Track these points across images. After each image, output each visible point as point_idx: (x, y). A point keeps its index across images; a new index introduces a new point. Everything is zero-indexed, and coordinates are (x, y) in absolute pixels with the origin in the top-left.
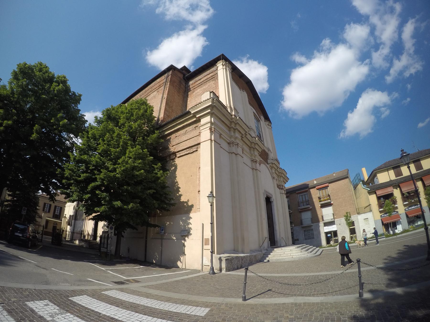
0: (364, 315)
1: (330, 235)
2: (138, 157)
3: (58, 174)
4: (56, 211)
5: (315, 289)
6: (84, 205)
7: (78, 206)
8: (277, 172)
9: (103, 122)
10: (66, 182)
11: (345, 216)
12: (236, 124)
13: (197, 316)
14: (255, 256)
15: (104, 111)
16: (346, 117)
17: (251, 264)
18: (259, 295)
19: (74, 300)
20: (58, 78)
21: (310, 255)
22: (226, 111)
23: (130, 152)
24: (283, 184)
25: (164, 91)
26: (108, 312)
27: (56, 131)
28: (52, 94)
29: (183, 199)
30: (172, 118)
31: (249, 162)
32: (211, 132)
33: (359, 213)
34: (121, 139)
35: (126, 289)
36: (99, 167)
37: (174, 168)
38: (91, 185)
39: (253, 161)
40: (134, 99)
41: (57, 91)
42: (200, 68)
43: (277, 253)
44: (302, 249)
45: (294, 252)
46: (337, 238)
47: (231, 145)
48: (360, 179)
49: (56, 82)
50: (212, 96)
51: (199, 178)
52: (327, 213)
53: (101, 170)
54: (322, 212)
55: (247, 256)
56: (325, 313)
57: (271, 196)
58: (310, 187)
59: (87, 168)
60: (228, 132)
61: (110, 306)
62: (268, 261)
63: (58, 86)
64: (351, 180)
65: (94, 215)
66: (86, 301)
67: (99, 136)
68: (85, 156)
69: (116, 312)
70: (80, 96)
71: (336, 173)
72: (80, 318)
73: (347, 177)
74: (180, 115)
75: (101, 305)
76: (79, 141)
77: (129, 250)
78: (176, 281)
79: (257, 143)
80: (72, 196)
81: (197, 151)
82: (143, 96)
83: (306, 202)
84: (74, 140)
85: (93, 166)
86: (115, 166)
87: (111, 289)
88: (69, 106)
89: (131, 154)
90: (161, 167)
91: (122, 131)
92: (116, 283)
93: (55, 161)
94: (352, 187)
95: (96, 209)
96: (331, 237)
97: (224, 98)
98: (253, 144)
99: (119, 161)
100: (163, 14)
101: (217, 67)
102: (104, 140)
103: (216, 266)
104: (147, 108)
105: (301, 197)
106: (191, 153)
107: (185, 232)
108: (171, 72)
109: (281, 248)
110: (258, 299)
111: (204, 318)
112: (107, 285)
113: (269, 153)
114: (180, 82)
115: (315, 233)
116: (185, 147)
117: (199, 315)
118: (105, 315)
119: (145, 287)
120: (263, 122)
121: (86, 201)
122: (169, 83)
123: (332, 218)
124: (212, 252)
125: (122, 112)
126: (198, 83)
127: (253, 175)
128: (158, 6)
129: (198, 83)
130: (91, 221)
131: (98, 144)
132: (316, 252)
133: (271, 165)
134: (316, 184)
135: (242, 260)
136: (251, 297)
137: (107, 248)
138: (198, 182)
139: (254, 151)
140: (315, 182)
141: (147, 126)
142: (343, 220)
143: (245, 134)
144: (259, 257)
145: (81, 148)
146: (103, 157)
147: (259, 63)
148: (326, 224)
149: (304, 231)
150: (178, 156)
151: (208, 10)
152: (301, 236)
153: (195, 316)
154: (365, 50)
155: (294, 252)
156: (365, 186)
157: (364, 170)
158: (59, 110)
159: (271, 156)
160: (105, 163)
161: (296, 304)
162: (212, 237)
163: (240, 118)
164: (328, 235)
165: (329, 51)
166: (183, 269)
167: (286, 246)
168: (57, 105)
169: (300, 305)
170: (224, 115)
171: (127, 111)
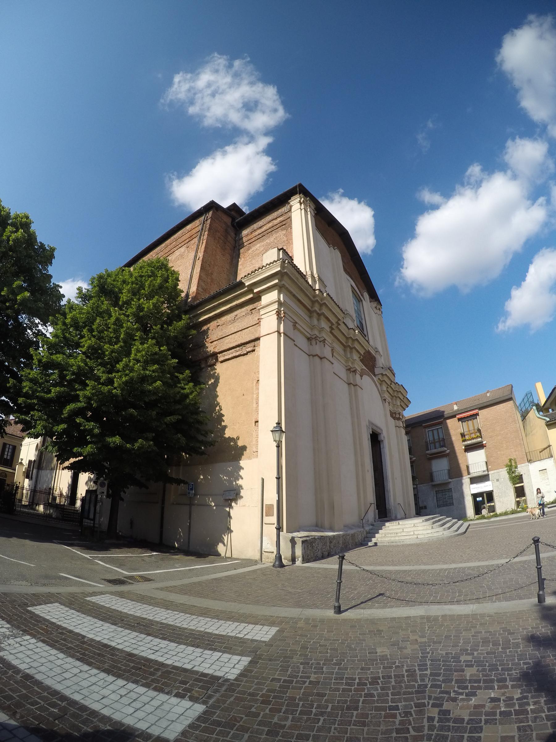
0: (549, 634)
1: (481, 499)
2: (152, 359)
3: (10, 387)
4: (6, 453)
5: (460, 592)
6: (54, 444)
7: (43, 445)
8: (390, 390)
9: (91, 297)
10: (25, 402)
11: (507, 466)
12: (321, 305)
13: (257, 641)
14: (353, 536)
15: (94, 278)
16: (508, 296)
17: (347, 548)
18: (362, 603)
19: (37, 612)
20: (16, 218)
21: (447, 533)
22: (305, 283)
23: (138, 351)
24: (400, 410)
25: (198, 246)
26: (99, 634)
27: (9, 311)
28: (5, 247)
29: (228, 434)
30: (212, 294)
31: (343, 373)
32: (279, 318)
33: (530, 461)
34: (123, 327)
35: (129, 592)
36: (82, 377)
37: (213, 381)
38: (68, 407)
39: (349, 370)
40: (145, 258)
41: (14, 240)
42: (261, 208)
43: (390, 530)
44: (434, 523)
45: (420, 528)
46: (492, 504)
47: (314, 342)
48: (533, 402)
49: (13, 225)
50: (281, 257)
51: (257, 399)
52: (476, 461)
53: (87, 381)
54: (466, 460)
55: (338, 536)
56: (481, 632)
57: (379, 431)
58: (446, 416)
59: (62, 377)
60: (307, 318)
61: (101, 622)
62: (376, 544)
63: (16, 232)
64: (518, 405)
65: (72, 460)
66: (58, 613)
67: (83, 323)
68: (58, 355)
69: (112, 634)
70: (53, 250)
71: (491, 392)
72: (47, 645)
73: (510, 399)
74: (226, 289)
75: (85, 620)
76: (49, 331)
77: (132, 523)
78: (215, 579)
79: (357, 340)
80: (35, 426)
81: (254, 351)
82: (162, 253)
83: (439, 441)
84: (40, 327)
85: (73, 373)
86: (110, 375)
87: (102, 593)
88: (34, 268)
89: (139, 354)
90: (189, 377)
91: (124, 314)
92: (110, 581)
93: (7, 364)
94: (519, 416)
95: (75, 450)
96: (483, 502)
97: (301, 260)
98: (350, 341)
99: (118, 366)
100: (201, 117)
101: (291, 207)
102: (91, 331)
103: (286, 552)
104: (168, 275)
105: (431, 434)
106: (244, 355)
107: (232, 492)
108: (211, 213)
109: (397, 522)
110: (362, 611)
111: (269, 644)
112: (95, 586)
113: (377, 356)
114: (226, 231)
115: (455, 495)
116: (234, 345)
117: (259, 639)
118: (92, 640)
119: (162, 589)
120: (367, 303)
121: (60, 436)
122: (206, 233)
123: (485, 469)
124: (279, 529)
125: (124, 282)
126: (257, 233)
127: (350, 394)
128: (192, 102)
129: (257, 233)
130: (66, 471)
131: (82, 337)
132: (459, 528)
133: (380, 377)
134: (456, 411)
135: (331, 542)
136: (350, 606)
137: (94, 520)
138: (255, 405)
139: (351, 352)
140: (456, 408)
141: (167, 307)
142: (504, 473)
143: (337, 323)
144: (360, 538)
145: (51, 343)
146: (91, 359)
147: (360, 202)
148: (474, 480)
149: (436, 493)
150: (220, 359)
151: (275, 110)
152: (431, 501)
153: (253, 641)
154: (539, 182)
155: (420, 528)
156: (541, 413)
157: (539, 386)
158: (16, 275)
159: (381, 361)
160: (94, 370)
161: (428, 618)
162: (279, 502)
163: (328, 294)
164: (478, 499)
165: (478, 185)
166: (226, 559)
167: (406, 517)
168: (13, 265)
169: (436, 618)
170: (301, 290)
171: (134, 279)
